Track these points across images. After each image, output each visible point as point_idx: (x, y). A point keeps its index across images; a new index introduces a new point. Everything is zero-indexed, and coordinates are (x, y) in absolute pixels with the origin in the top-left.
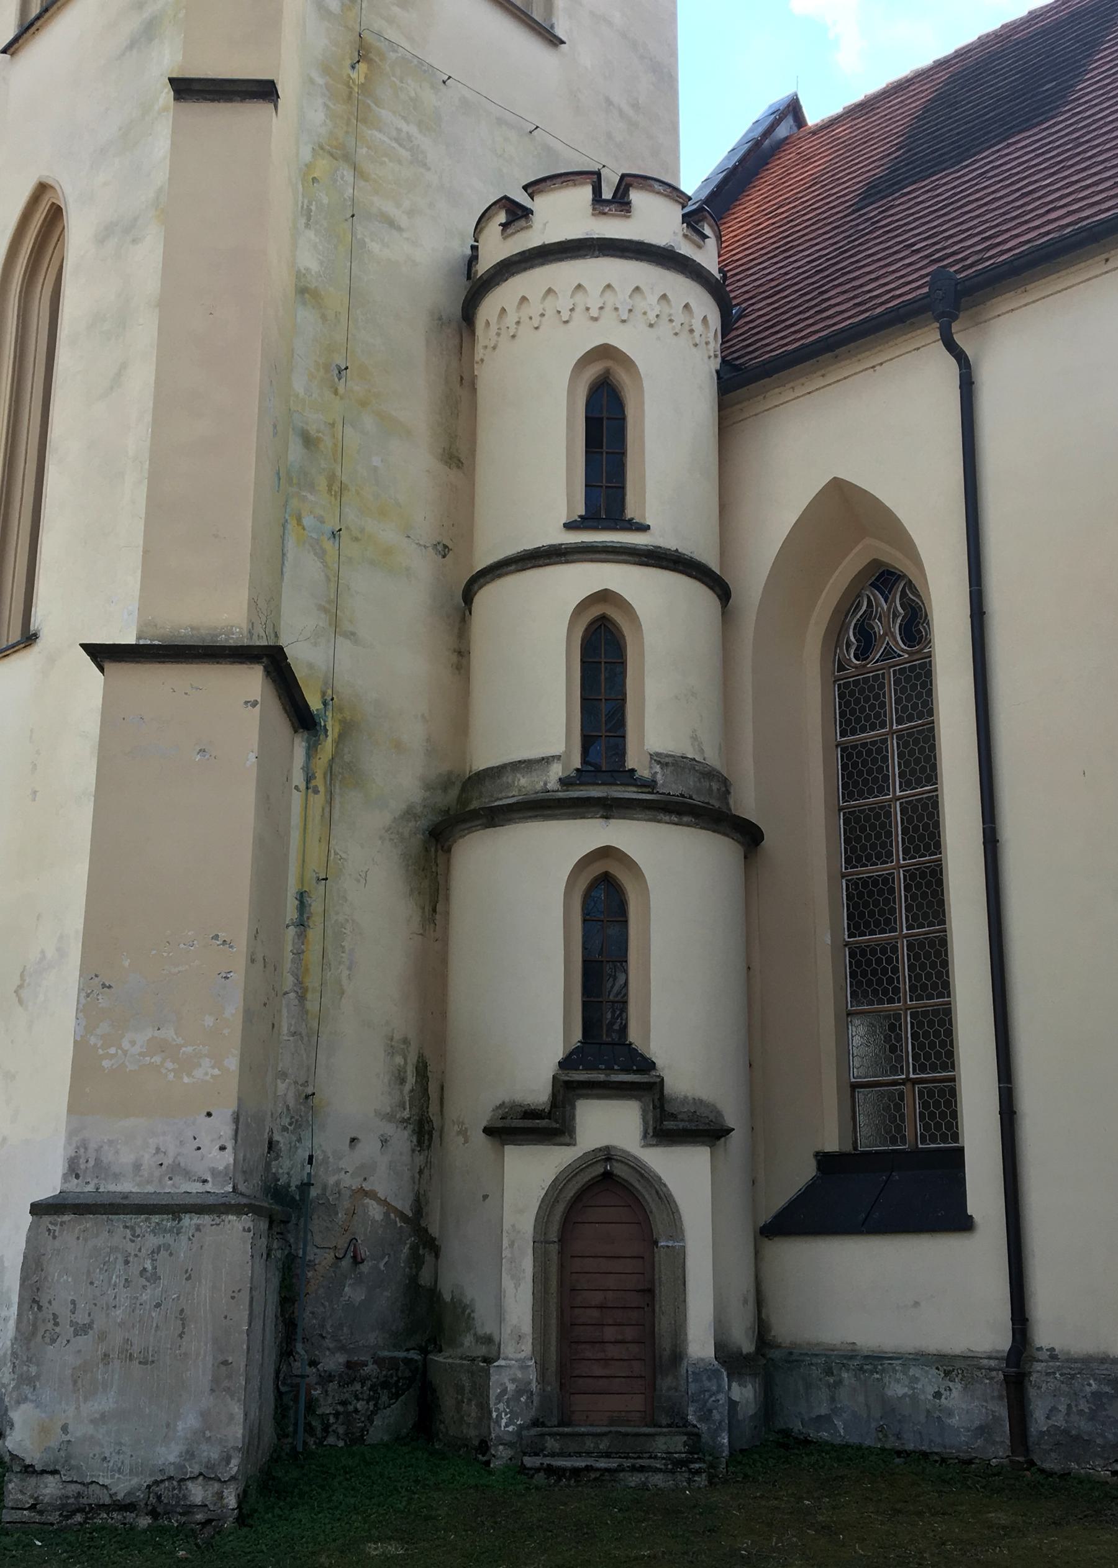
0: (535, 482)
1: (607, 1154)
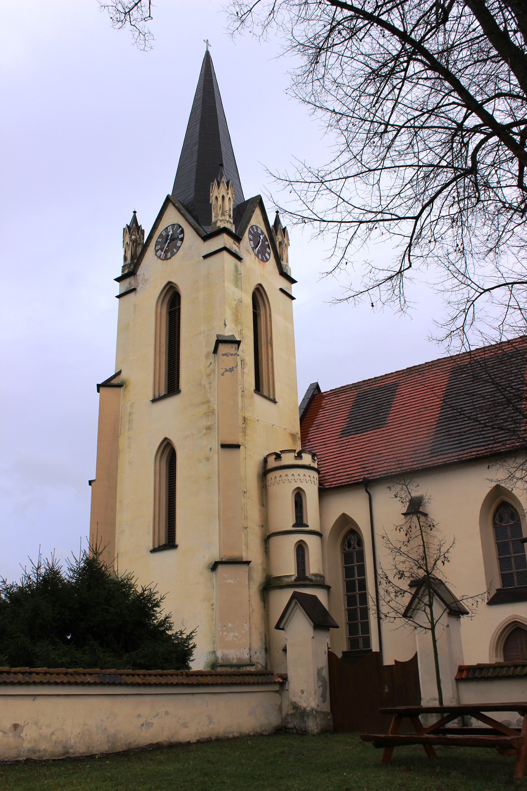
0: (285, 518)
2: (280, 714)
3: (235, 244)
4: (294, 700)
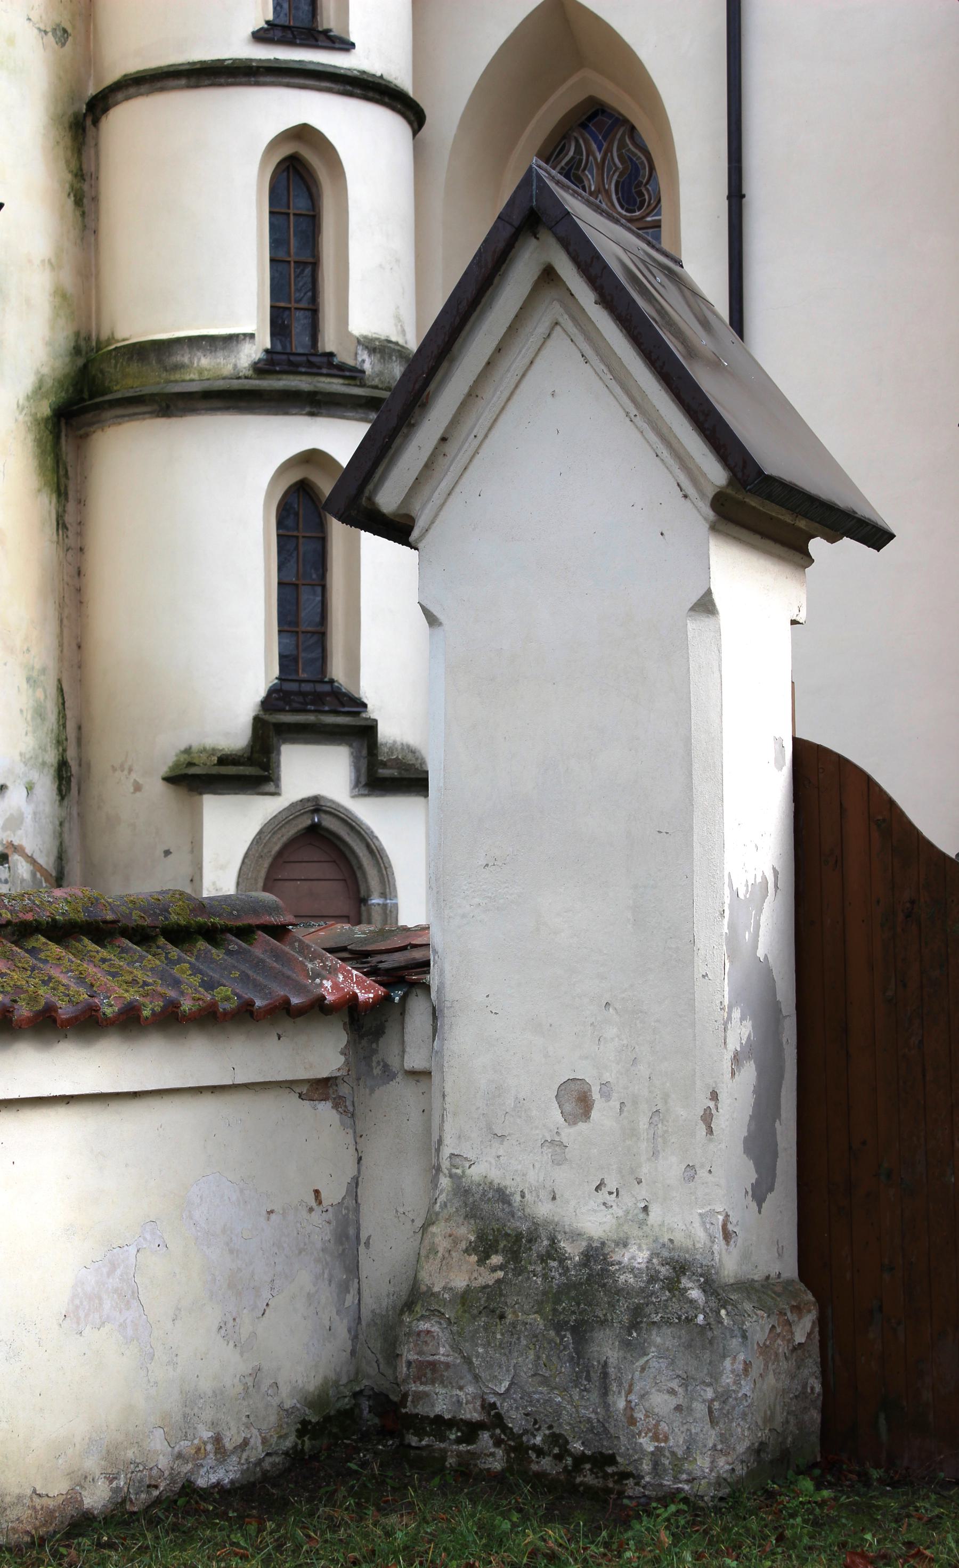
1: (316, 805)
2: (344, 1288)
4: (486, 1167)
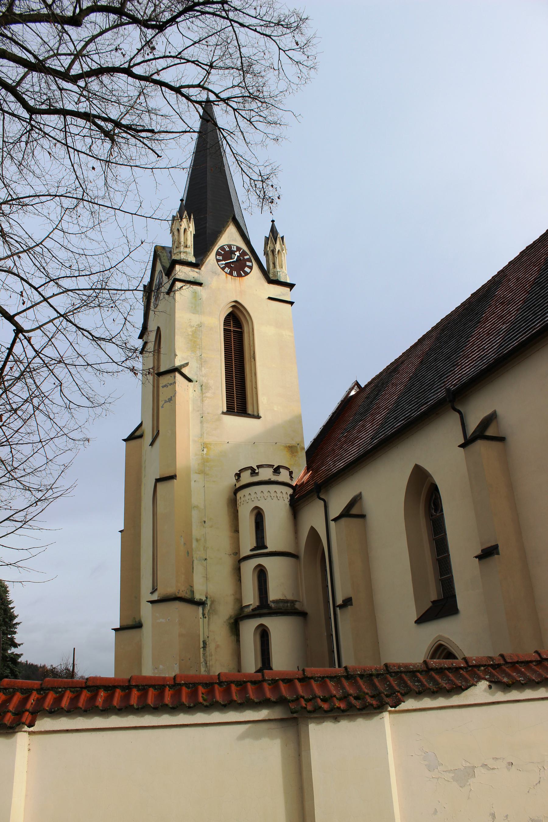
3: (194, 271)
